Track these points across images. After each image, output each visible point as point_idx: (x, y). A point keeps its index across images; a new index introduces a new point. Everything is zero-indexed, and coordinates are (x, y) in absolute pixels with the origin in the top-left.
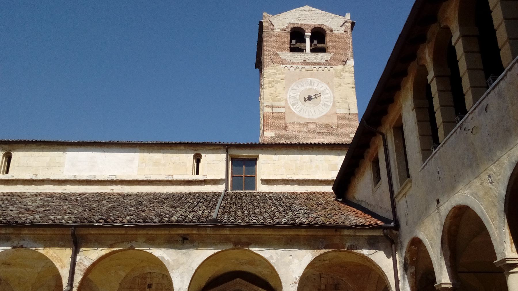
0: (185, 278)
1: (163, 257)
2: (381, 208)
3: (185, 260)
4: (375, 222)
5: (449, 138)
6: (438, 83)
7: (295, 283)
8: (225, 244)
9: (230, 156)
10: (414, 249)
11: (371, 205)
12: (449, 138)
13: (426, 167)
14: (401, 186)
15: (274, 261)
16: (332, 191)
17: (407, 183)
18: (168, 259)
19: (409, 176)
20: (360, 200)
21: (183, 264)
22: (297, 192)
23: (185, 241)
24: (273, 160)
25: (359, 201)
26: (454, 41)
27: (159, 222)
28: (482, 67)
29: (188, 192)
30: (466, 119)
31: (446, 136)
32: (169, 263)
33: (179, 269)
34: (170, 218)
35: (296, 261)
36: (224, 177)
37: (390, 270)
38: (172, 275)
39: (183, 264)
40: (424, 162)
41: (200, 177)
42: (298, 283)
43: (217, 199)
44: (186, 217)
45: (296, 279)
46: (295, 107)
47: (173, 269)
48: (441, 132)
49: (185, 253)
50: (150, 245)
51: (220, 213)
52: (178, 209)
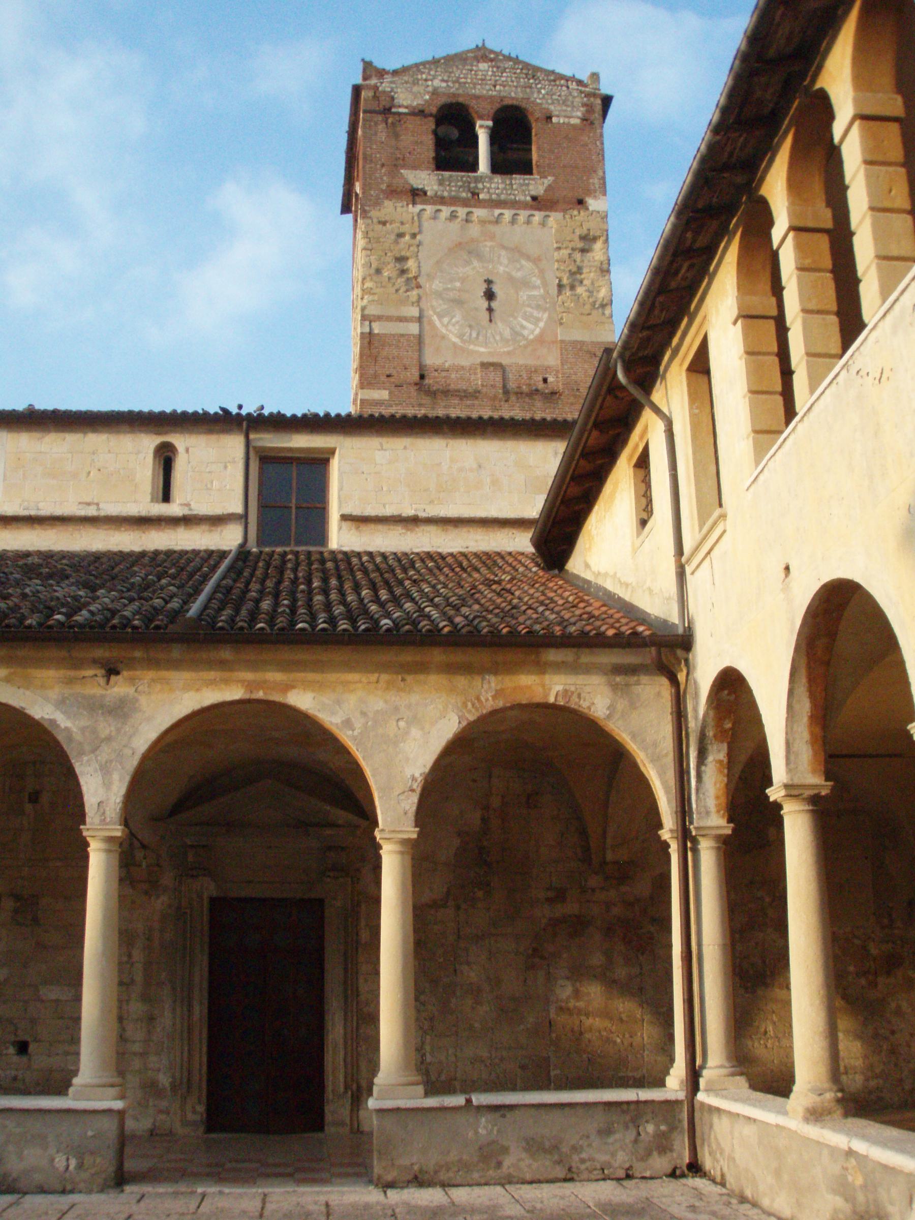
0: (116, 776)
1: (53, 722)
2: (650, 590)
3: (113, 729)
4: (631, 629)
5: (818, 398)
6: (799, 247)
7: (413, 790)
8: (223, 686)
9: (258, 450)
10: (728, 697)
11: (627, 585)
12: (818, 398)
13: (761, 477)
14: (700, 530)
15: (356, 733)
16: (531, 549)
17: (715, 523)
18: (68, 724)
19: (721, 505)
20: (603, 571)
21: (109, 739)
22: (440, 550)
23: (113, 678)
24: (376, 464)
25: (599, 573)
26: (838, 129)
27: (40, 625)
28: (907, 206)
29: (137, 548)
30: (862, 344)
31: (812, 391)
32: (70, 739)
33: (98, 752)
34: (72, 616)
35: (415, 732)
36: (238, 509)
37: (666, 755)
38: (78, 768)
39: (109, 739)
40: (757, 463)
41: (174, 509)
42: (419, 790)
43: (214, 569)
44: (114, 613)
45: (414, 779)
46: (446, 320)
47: (82, 753)
48: (800, 381)
49: (112, 711)
50: (19, 688)
51: (215, 604)
52: (101, 592)
